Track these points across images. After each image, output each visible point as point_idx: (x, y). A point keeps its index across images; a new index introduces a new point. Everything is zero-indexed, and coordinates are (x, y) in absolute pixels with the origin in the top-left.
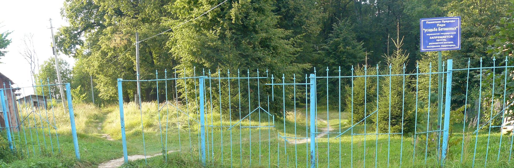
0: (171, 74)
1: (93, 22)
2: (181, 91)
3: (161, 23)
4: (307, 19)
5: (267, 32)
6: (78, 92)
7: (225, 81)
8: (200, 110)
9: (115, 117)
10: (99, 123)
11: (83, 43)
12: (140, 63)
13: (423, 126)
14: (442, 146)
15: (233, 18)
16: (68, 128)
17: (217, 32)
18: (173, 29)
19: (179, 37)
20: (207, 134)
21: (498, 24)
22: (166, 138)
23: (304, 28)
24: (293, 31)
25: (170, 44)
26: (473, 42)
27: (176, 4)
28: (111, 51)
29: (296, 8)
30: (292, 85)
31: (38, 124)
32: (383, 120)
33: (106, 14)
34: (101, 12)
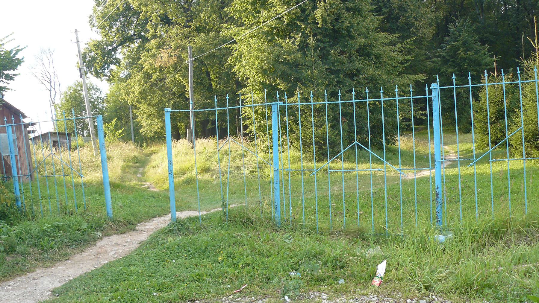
0: (234, 101)
1: (132, 34)
2: (247, 122)
3: (221, 32)
4: (416, 20)
5: (366, 37)
6: (113, 127)
7: (307, 108)
8: (272, 148)
9: (161, 159)
10: (140, 167)
11: (119, 63)
12: (194, 88)
15: (320, 21)
16: (98, 175)
17: (297, 40)
18: (237, 40)
20: (282, 180)
22: (228, 187)
23: (413, 31)
24: (399, 35)
25: (232, 61)
28: (156, 72)
31: (57, 171)
33: (150, 22)
34: (142, 20)
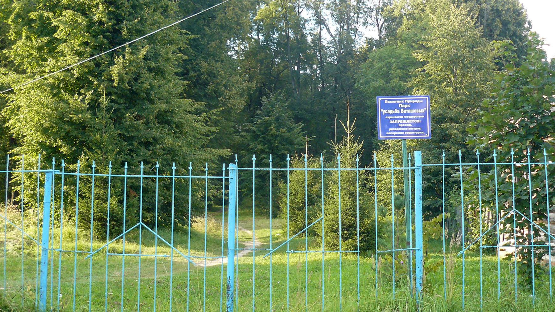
5: (167, 102)
13: (386, 241)
14: (415, 272)
17: (87, 98)
19: (23, 102)
21: (479, 107)
23: (222, 100)
24: (205, 103)
25: (7, 113)
26: (448, 129)
27: (15, 48)
29: (210, 72)
30: (203, 179)
32: (331, 232)
